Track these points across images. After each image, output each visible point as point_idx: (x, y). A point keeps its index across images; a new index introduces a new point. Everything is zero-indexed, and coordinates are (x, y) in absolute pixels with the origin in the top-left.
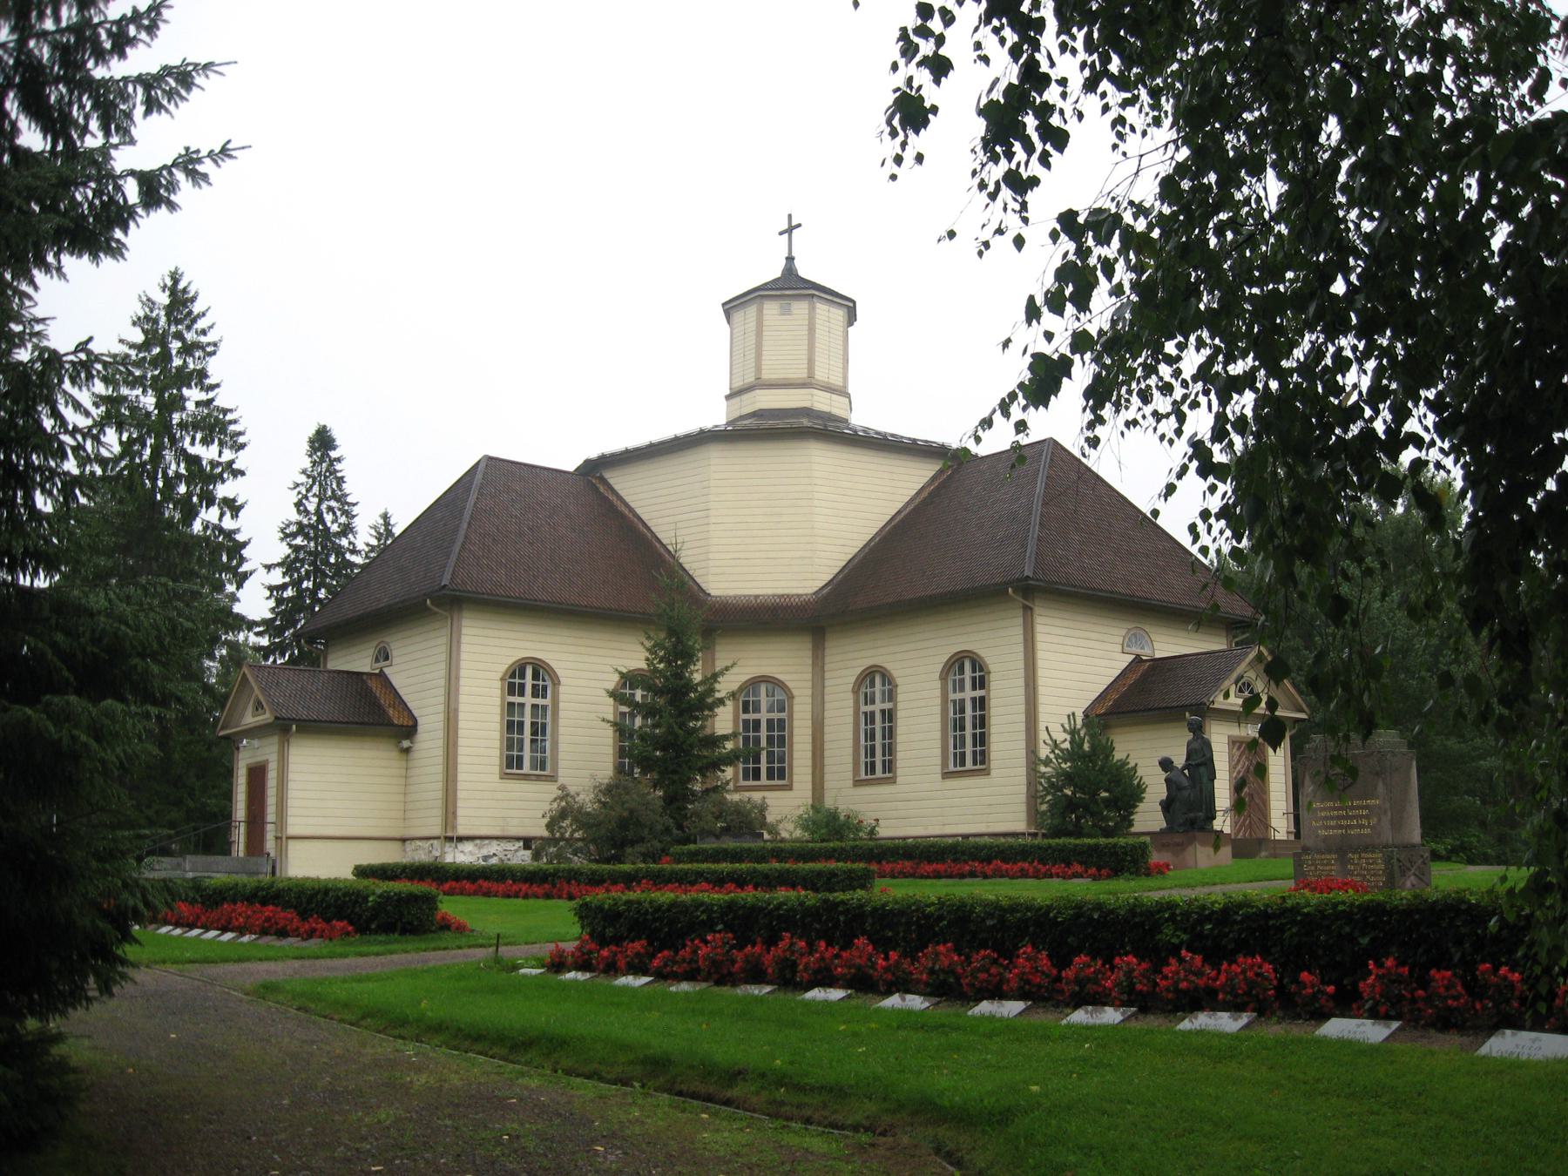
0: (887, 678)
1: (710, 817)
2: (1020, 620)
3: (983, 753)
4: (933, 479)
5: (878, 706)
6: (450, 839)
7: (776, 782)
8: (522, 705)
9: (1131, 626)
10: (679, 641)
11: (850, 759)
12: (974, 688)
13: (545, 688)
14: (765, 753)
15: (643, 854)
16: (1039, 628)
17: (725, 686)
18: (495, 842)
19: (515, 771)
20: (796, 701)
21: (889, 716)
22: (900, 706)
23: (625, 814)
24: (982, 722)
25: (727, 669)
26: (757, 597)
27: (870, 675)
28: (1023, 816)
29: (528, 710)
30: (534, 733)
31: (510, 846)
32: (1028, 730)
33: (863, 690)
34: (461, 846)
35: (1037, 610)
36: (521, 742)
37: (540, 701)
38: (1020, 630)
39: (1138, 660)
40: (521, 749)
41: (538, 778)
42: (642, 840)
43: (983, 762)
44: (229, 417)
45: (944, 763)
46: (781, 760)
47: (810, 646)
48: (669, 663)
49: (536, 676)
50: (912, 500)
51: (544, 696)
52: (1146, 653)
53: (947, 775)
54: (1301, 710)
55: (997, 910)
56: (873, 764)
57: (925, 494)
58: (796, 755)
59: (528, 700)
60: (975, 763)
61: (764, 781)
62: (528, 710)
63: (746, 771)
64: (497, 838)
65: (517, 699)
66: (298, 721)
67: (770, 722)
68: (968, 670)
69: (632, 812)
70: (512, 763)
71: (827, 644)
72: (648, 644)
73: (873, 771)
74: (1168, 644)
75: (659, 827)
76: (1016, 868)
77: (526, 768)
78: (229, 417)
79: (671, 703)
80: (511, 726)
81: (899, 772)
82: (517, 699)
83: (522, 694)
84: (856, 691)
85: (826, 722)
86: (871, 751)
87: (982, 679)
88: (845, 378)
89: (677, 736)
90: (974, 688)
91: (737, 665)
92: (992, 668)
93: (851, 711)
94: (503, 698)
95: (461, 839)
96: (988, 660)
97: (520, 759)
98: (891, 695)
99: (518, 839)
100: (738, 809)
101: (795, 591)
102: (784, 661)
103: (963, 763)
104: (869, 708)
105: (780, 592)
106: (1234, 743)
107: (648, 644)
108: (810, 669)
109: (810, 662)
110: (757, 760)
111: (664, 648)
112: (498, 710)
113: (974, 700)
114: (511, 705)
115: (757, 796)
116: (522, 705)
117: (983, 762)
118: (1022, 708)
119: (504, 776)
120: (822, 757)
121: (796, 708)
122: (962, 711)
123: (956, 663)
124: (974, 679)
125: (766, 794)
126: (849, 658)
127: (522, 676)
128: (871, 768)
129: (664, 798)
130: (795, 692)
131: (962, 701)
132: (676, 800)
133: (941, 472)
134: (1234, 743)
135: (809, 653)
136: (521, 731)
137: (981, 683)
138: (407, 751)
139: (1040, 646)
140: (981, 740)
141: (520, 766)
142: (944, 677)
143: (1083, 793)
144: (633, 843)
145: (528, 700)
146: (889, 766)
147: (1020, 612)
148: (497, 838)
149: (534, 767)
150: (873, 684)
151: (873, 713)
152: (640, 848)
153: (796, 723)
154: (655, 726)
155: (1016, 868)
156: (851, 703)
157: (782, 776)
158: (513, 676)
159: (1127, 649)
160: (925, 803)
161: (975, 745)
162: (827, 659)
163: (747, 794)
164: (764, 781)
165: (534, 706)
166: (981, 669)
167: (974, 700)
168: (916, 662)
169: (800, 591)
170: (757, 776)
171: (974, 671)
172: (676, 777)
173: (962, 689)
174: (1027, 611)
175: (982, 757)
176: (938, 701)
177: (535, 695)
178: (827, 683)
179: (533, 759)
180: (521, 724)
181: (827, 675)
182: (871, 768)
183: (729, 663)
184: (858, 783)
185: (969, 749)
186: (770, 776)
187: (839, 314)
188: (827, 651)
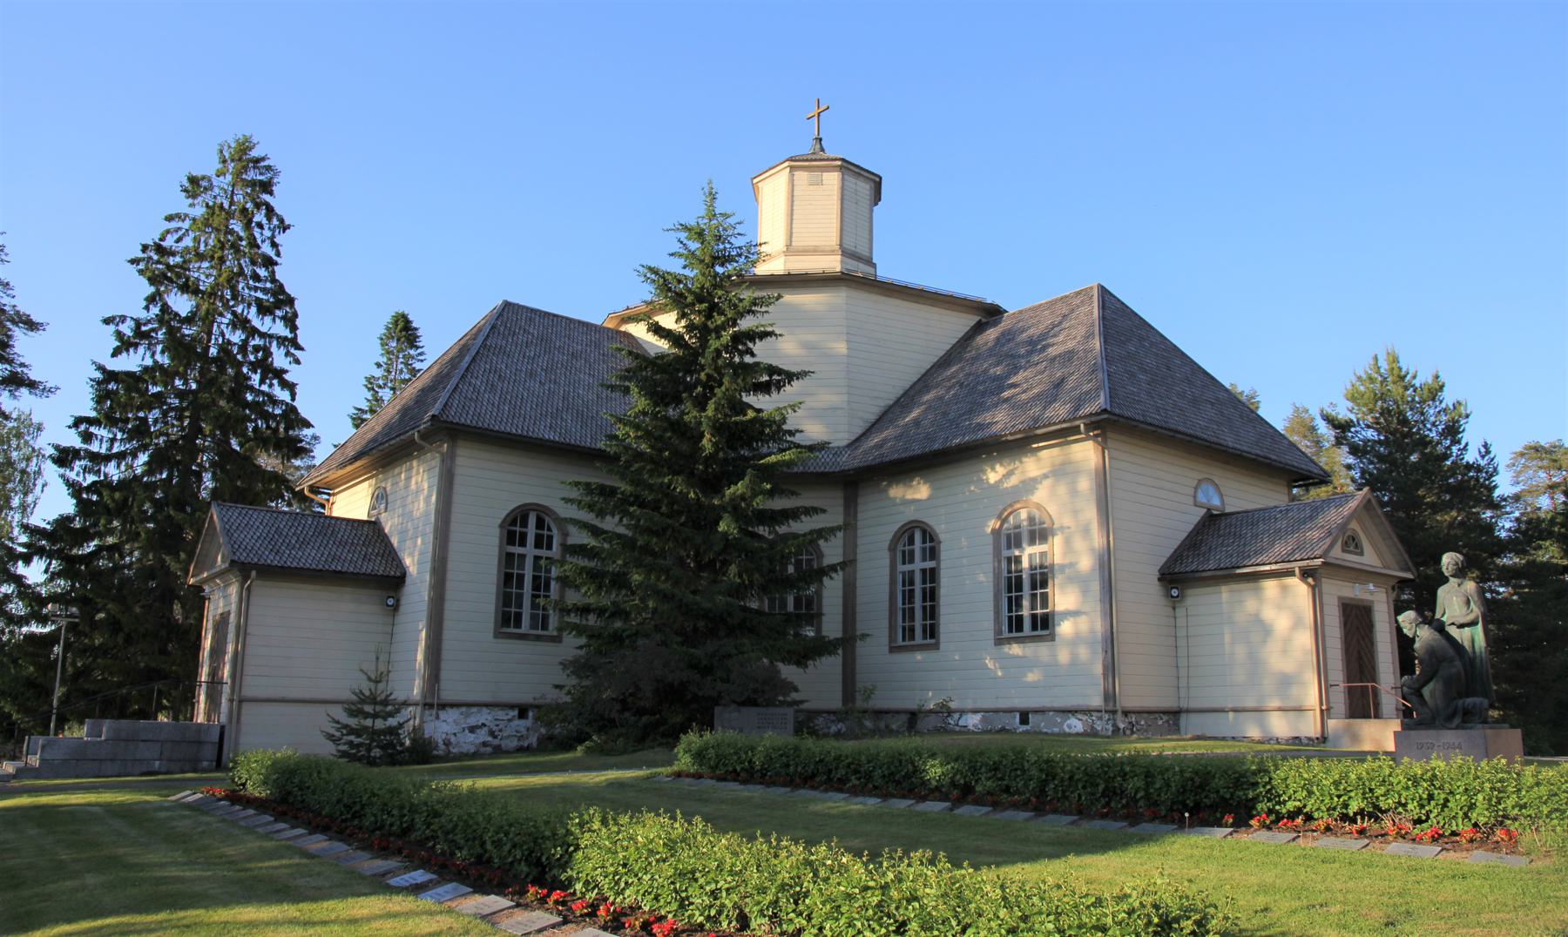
5: (918, 565)
6: (431, 706)
8: (522, 557)
12: (924, 559)
13: (550, 538)
18: (485, 710)
19: (512, 630)
21: (932, 576)
22: (943, 565)
24: (931, 595)
29: (529, 563)
30: (536, 587)
31: (501, 714)
33: (900, 548)
34: (443, 715)
36: (520, 597)
37: (543, 553)
40: (520, 606)
41: (538, 638)
43: (933, 636)
44: (731, 221)
45: (998, 632)
49: (540, 524)
51: (549, 547)
54: (1408, 569)
55: (158, 910)
59: (530, 550)
62: (529, 563)
64: (487, 705)
65: (517, 550)
66: (256, 566)
70: (507, 619)
77: (525, 626)
78: (731, 221)
80: (507, 579)
81: (943, 638)
82: (517, 550)
83: (523, 543)
84: (892, 549)
86: (909, 614)
88: (871, 249)
90: (924, 559)
92: (942, 537)
94: (501, 547)
95: (443, 706)
97: (519, 616)
99: (512, 707)
103: (912, 638)
112: (495, 561)
113: (924, 571)
114: (510, 556)
116: (522, 557)
117: (933, 636)
119: (498, 635)
122: (912, 583)
124: (924, 550)
127: (525, 524)
136: (520, 585)
138: (396, 608)
141: (518, 624)
145: (530, 550)
146: (932, 632)
148: (487, 705)
149: (534, 626)
150: (911, 541)
158: (514, 523)
161: (924, 619)
165: (537, 558)
166: (932, 540)
167: (924, 571)
171: (924, 542)
173: (912, 561)
177: (538, 545)
179: (533, 617)
180: (521, 578)
182: (909, 632)
187: (865, 188)
188: (860, 508)
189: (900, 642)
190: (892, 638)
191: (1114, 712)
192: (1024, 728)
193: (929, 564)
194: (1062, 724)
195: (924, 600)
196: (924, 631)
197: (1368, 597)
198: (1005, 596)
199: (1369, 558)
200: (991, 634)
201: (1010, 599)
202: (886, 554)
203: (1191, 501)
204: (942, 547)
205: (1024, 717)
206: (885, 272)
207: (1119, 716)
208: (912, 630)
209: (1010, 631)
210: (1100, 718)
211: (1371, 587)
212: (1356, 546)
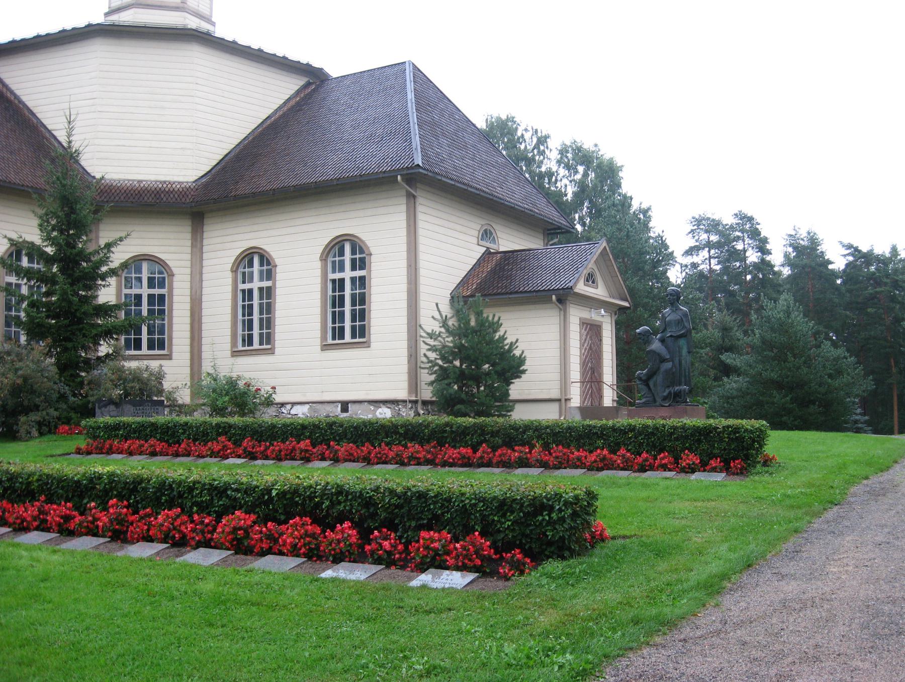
0: (265, 259)
1: (109, 385)
2: (404, 208)
3: (269, 335)
4: (298, 92)
5: (256, 285)
7: (156, 352)
9: (483, 222)
10: (73, 211)
11: (228, 332)
12: (261, 280)
14: (146, 324)
15: (40, 424)
16: (421, 217)
17: (118, 257)
20: (175, 279)
21: (268, 293)
22: (278, 284)
23: (20, 381)
24: (361, 300)
25: (121, 239)
26: (140, 181)
27: (248, 257)
28: (405, 385)
32: (409, 306)
33: (241, 270)
35: (420, 200)
38: (403, 216)
39: (488, 254)
42: (37, 408)
43: (268, 343)
46: (162, 332)
47: (189, 229)
48: (61, 232)
50: (280, 108)
52: (493, 247)
53: (325, 347)
54: (626, 300)
56: (250, 337)
57: (293, 103)
58: (175, 327)
60: (261, 344)
61: (145, 350)
63: (127, 341)
67: (151, 297)
68: (347, 252)
69: (26, 379)
71: (206, 228)
72: (41, 212)
73: (250, 343)
74: (509, 240)
75: (55, 396)
76: (592, 458)
79: (62, 270)
81: (373, 338)
84: (234, 270)
85: (204, 298)
86: (338, 317)
87: (363, 260)
88: (211, 9)
89: (70, 303)
90: (261, 280)
91: (127, 242)
93: (229, 288)
96: (369, 243)
98: (269, 275)
100: (136, 376)
101: (176, 179)
102: (164, 242)
103: (342, 337)
104: (247, 286)
105: (162, 178)
106: (583, 323)
107: (41, 212)
108: (189, 250)
109: (189, 243)
110: (139, 331)
111: (57, 217)
115: (154, 364)
118: (404, 287)
120: (200, 330)
121: (175, 285)
123: (336, 246)
125: (163, 362)
126: (227, 241)
128: (339, 333)
129: (58, 364)
130: (175, 270)
131: (342, 281)
132: (69, 367)
133: (308, 85)
134: (583, 323)
135: (189, 236)
137: (360, 263)
139: (421, 232)
140: (360, 315)
142: (324, 258)
143: (473, 369)
144: (27, 411)
146: (268, 338)
147: (404, 200)
150: (251, 264)
151: (250, 291)
152: (35, 417)
153: (175, 299)
154: (48, 294)
155: (592, 458)
156: (229, 281)
157: (161, 346)
159: (481, 243)
160: (304, 375)
161: (261, 328)
162: (205, 242)
163: (146, 362)
164: (145, 350)
166: (269, 263)
167: (353, 280)
168: (296, 245)
169: (181, 179)
170: (138, 346)
171: (262, 265)
172: (70, 345)
173: (342, 269)
174: (411, 198)
175: (361, 332)
176: (319, 280)
178: (205, 263)
181: (205, 256)
182: (249, 340)
183: (123, 234)
184: (235, 353)
185: (348, 324)
186: (151, 347)
188: (205, 235)
189: (240, 348)
190: (234, 343)
191: (416, 402)
192: (345, 415)
193: (266, 284)
194: (375, 411)
195: (261, 313)
196: (244, 340)
197: (599, 318)
198: (330, 310)
199: (599, 292)
200: (318, 342)
201: (334, 313)
202: (229, 275)
203: (476, 242)
204: (278, 269)
205: (345, 406)
206: (220, 32)
207: (419, 406)
208: (342, 329)
209: (334, 338)
210: (405, 407)
211: (603, 311)
212: (593, 282)
